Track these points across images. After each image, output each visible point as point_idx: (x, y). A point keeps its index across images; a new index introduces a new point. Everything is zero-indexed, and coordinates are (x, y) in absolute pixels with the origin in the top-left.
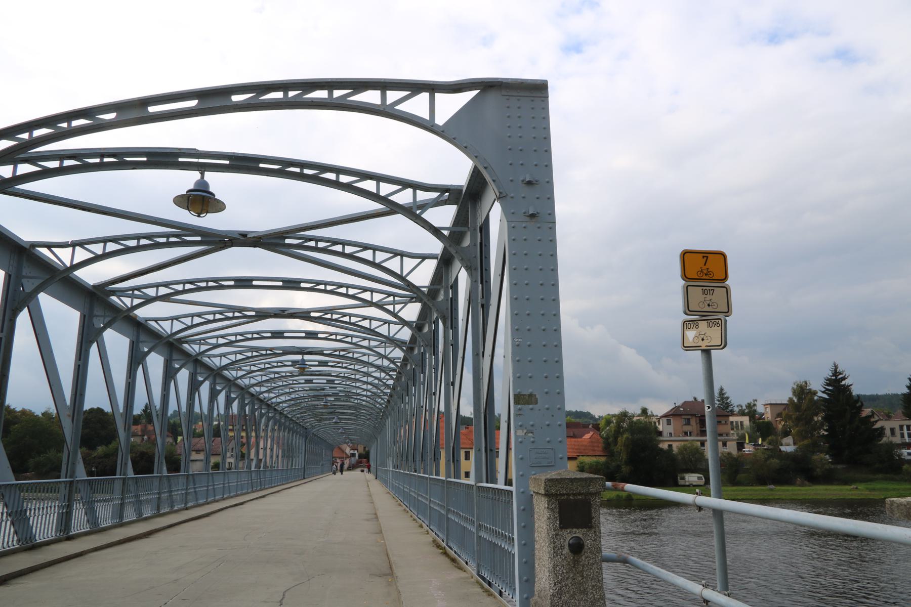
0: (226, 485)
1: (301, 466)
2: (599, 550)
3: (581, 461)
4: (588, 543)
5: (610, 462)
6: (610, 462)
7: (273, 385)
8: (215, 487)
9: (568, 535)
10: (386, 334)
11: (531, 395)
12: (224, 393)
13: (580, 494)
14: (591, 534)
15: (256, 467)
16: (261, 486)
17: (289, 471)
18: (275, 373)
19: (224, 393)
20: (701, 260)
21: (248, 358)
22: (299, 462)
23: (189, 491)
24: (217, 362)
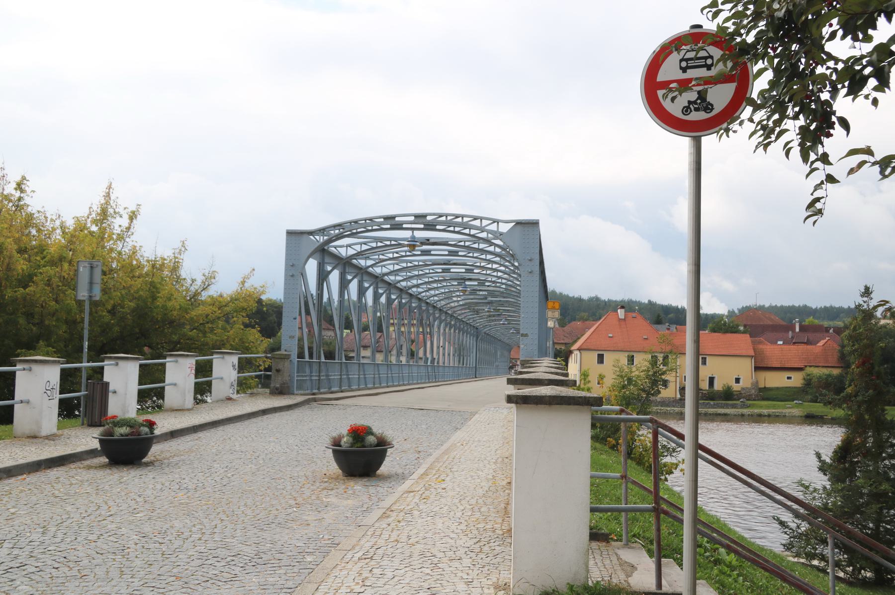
0: (390, 375)
1: (473, 365)
3: (809, 373)
5: (845, 375)
6: (845, 375)
7: (381, 257)
8: (381, 376)
11: (526, 334)
12: (355, 282)
15: (431, 363)
16: (435, 379)
17: (464, 369)
18: (407, 262)
19: (384, 296)
21: (373, 248)
22: (471, 360)
23: (322, 378)
24: (343, 252)
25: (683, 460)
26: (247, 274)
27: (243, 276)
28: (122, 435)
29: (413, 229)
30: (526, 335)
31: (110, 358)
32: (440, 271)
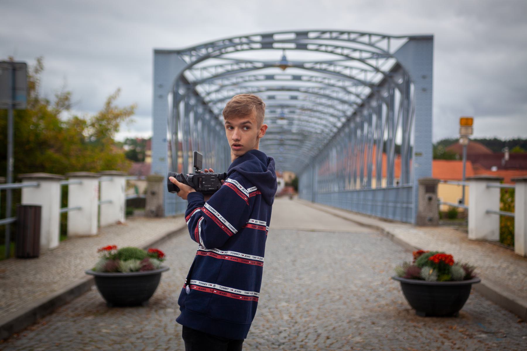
25: (301, 279)
28: (131, 271)
29: (284, 49)
31: (31, 179)
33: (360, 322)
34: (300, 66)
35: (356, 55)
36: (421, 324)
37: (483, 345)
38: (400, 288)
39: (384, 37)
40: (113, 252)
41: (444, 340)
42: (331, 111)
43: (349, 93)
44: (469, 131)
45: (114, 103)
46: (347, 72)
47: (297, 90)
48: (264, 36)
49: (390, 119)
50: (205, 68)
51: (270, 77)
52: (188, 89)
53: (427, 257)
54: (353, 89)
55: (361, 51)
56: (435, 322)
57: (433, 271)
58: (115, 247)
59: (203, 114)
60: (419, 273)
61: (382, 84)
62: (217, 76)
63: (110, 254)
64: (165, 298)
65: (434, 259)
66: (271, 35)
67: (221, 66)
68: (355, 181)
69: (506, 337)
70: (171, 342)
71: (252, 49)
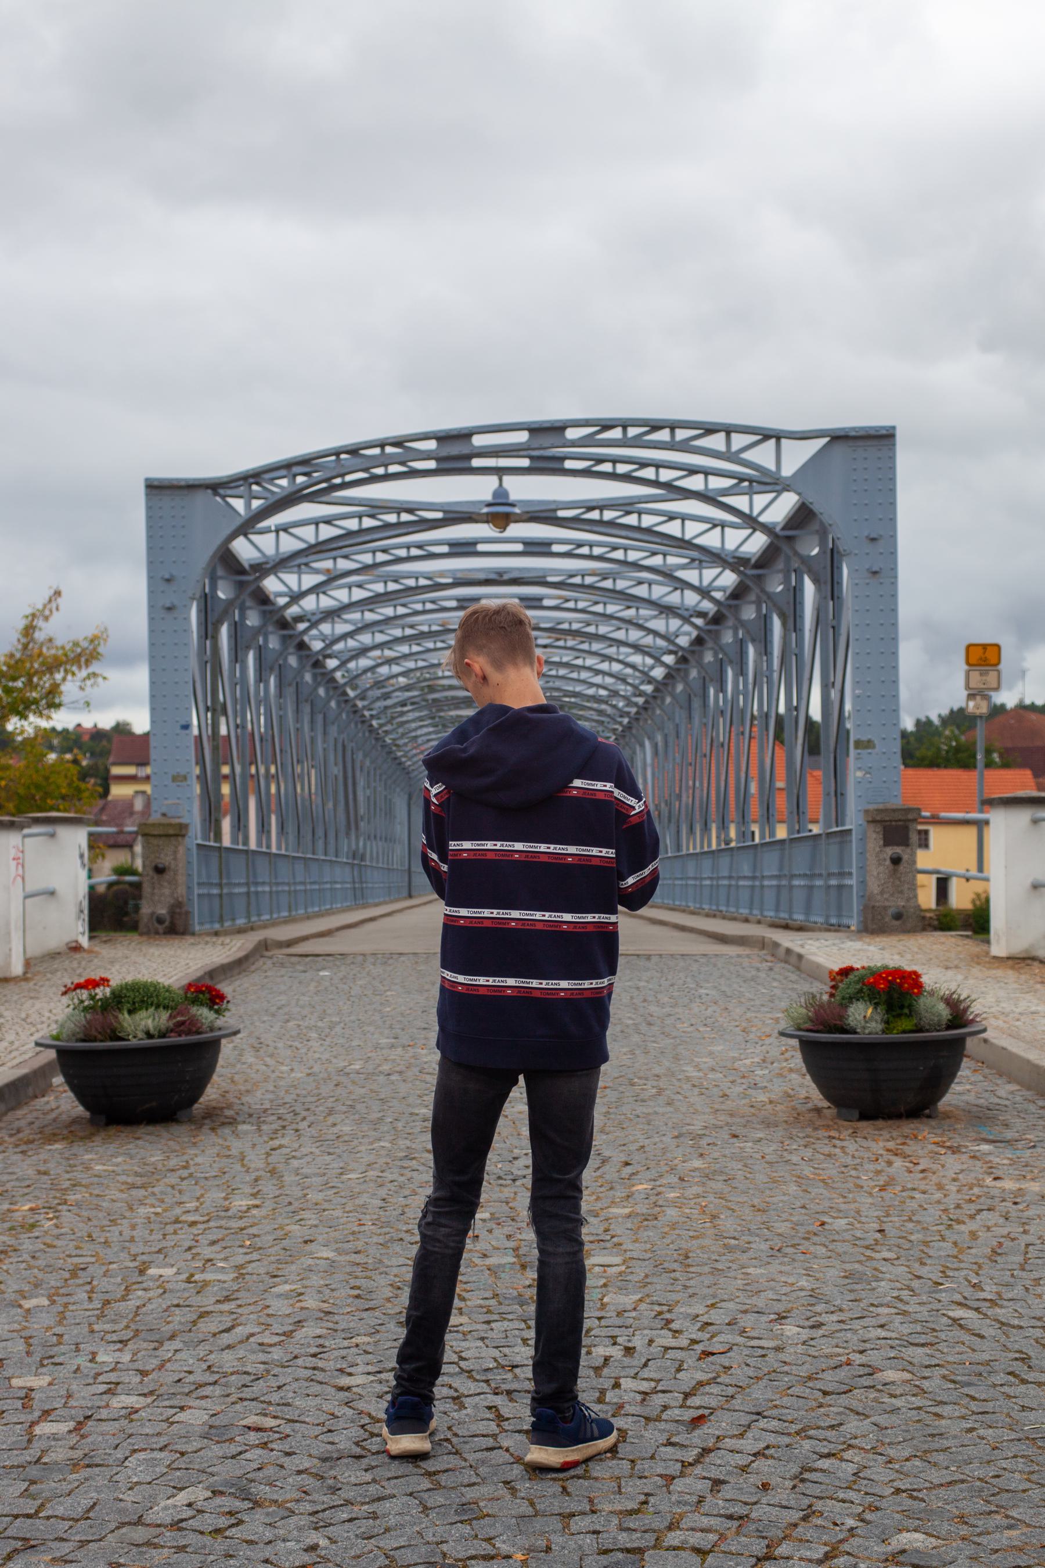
2: (914, 862)
4: (905, 857)
9: (890, 851)
10: (747, 510)
11: (869, 741)
13: (900, 820)
14: (908, 850)
20: (980, 650)
26: (40, 607)
27: (29, 611)
28: (149, 1035)
29: (500, 472)
30: (868, 744)
32: (453, 604)
33: (701, 1136)
34: (544, 515)
35: (696, 483)
36: (845, 1134)
37: (978, 1163)
38: (797, 1060)
39: (766, 435)
40: (101, 992)
41: (893, 1158)
42: (634, 635)
43: (684, 585)
44: (992, 676)
45: (45, 631)
46: (673, 528)
47: (540, 581)
48: (444, 438)
49: (791, 654)
50: (285, 528)
51: (463, 548)
52: (241, 585)
53: (861, 980)
54: (691, 576)
55: (707, 472)
56: (880, 1129)
57: (875, 1008)
58: (104, 981)
59: (283, 653)
60: (841, 1017)
61: (766, 559)
62: (319, 549)
63: (92, 998)
64: (230, 1106)
65: (876, 983)
66: (466, 435)
67: (328, 521)
68: (706, 828)
69: (1034, 1147)
70: (259, 1182)
71: (414, 473)
